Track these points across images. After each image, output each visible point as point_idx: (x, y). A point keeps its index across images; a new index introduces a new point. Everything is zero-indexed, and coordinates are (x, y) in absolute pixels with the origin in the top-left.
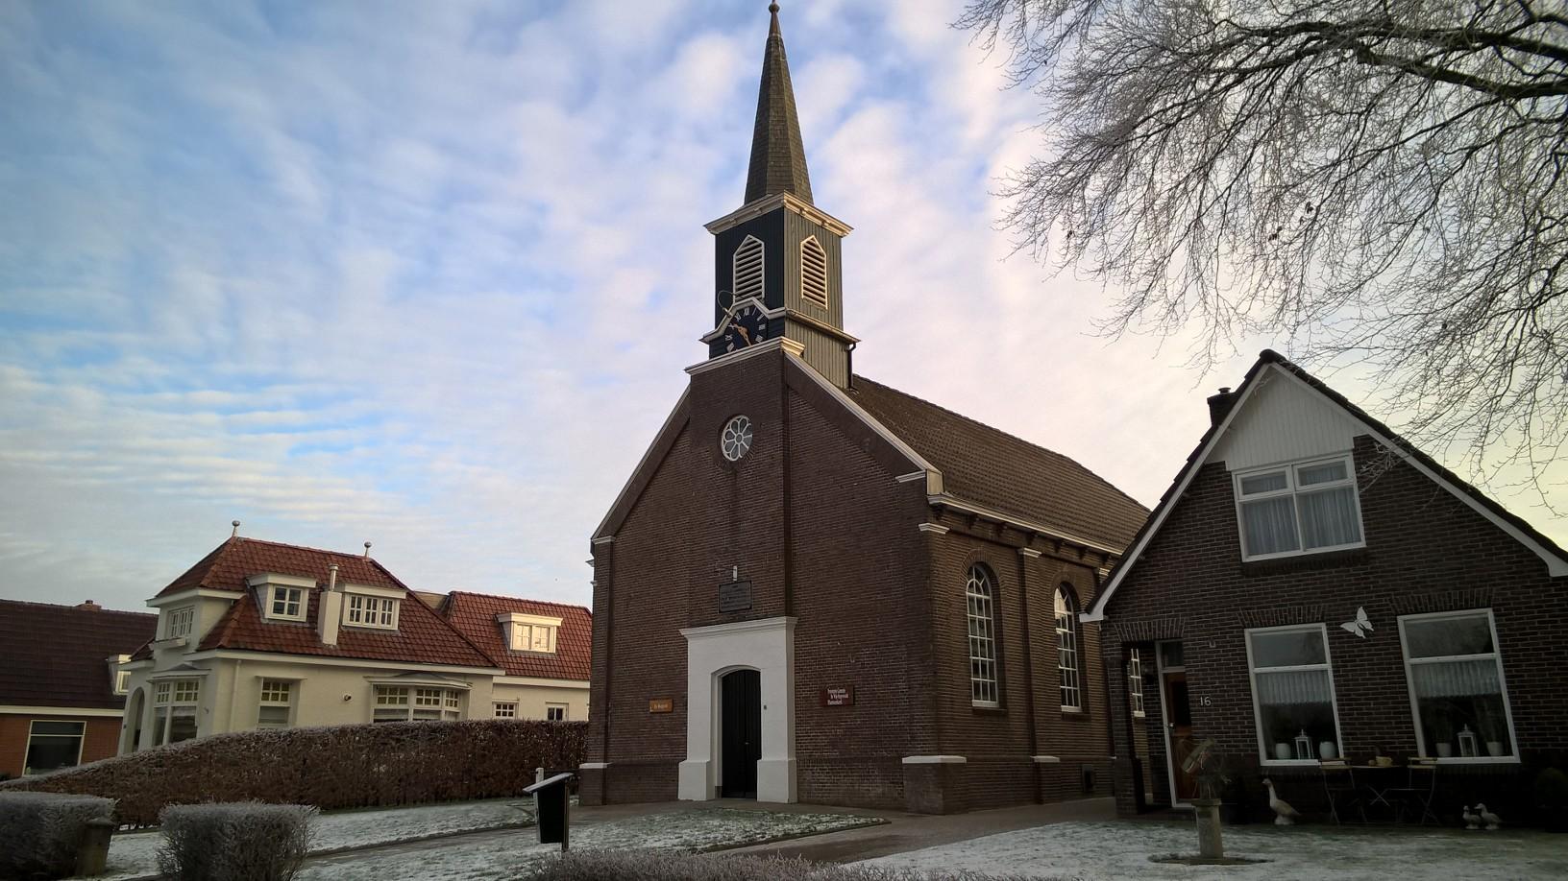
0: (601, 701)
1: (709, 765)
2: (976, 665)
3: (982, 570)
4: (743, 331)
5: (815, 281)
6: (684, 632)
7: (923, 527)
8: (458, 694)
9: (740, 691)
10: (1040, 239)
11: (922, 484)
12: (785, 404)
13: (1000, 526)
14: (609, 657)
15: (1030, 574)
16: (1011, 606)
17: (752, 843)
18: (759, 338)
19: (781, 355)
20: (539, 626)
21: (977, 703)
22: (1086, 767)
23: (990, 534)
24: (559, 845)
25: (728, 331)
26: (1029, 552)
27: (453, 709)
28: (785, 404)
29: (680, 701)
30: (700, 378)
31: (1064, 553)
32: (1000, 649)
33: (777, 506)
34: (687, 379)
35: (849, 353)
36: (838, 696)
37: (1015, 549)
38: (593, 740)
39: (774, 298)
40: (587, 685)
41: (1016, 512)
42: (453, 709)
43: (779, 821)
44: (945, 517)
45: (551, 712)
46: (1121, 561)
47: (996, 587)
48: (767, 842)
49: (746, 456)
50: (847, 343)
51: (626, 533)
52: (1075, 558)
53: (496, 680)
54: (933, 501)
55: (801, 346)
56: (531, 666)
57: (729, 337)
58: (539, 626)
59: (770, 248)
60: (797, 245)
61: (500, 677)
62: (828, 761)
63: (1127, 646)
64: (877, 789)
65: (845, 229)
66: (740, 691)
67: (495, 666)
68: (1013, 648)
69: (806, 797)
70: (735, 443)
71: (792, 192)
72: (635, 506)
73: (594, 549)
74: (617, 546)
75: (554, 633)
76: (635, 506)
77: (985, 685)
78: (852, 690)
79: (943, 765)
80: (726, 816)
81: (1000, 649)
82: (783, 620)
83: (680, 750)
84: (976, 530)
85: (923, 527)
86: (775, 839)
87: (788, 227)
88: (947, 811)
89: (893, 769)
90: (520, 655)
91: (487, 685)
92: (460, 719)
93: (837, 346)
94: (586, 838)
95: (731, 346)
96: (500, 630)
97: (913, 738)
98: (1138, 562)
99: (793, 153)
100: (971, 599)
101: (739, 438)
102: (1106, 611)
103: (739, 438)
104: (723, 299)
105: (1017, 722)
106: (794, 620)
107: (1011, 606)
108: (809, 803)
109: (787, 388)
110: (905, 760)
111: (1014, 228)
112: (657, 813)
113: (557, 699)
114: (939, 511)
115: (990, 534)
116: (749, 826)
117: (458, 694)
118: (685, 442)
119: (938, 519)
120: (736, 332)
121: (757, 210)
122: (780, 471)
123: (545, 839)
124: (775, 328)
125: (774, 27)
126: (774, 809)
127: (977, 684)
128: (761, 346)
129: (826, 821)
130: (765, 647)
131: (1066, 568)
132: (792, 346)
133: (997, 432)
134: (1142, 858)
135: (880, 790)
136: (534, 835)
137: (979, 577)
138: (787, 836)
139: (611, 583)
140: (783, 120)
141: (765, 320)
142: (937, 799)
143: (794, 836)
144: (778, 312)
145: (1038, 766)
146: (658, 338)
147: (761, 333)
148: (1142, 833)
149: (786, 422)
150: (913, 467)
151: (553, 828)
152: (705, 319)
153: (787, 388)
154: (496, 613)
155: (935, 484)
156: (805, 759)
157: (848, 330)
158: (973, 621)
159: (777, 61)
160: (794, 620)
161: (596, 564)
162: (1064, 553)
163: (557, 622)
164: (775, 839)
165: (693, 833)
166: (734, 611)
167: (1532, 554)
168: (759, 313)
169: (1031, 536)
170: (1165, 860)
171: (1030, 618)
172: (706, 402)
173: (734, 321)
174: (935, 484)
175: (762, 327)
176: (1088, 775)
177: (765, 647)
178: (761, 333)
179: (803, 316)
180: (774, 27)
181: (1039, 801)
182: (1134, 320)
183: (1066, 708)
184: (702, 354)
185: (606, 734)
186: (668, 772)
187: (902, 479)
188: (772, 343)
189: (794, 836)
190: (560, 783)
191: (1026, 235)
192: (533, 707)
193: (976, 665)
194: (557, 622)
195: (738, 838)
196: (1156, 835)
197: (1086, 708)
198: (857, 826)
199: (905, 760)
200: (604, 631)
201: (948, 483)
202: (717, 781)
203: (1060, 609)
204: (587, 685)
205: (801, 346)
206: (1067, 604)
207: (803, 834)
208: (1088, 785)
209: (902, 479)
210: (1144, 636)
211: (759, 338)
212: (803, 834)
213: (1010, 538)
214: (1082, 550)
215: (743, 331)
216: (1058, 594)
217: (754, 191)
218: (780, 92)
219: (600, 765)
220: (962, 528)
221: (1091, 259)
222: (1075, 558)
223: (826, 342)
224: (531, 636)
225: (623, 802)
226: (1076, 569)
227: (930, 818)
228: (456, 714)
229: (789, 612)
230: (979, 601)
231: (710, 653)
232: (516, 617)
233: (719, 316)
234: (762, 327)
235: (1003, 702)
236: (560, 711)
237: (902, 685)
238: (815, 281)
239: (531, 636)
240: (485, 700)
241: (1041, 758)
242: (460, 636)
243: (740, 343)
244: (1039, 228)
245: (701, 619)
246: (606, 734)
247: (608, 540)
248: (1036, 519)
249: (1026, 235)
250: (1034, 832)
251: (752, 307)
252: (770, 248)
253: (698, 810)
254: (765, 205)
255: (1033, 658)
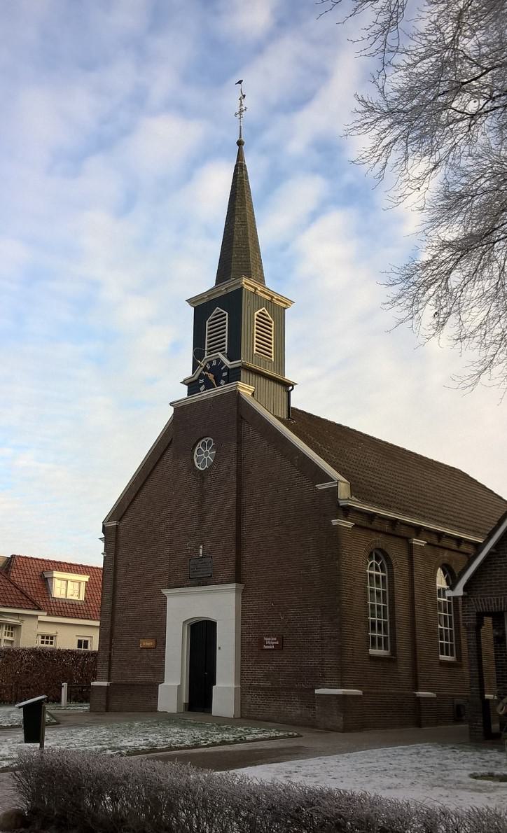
0: (108, 636)
1: (179, 687)
2: (373, 624)
3: (380, 554)
4: (211, 376)
5: (264, 338)
6: (164, 592)
7: (335, 522)
8: (13, 628)
9: (202, 633)
10: (416, 316)
11: (335, 491)
12: (239, 430)
13: (394, 522)
14: (113, 607)
15: (417, 558)
16: (401, 582)
17: (197, 746)
18: (222, 382)
19: (237, 395)
20: (72, 581)
21: (373, 651)
22: (458, 701)
23: (387, 528)
24: (38, 745)
25: (201, 376)
26: (418, 542)
27: (10, 638)
28: (239, 430)
29: (160, 640)
30: (180, 410)
31: (444, 542)
32: (392, 612)
33: (231, 503)
34: (171, 410)
35: (289, 393)
36: (271, 642)
37: (407, 539)
38: (102, 666)
39: (234, 354)
40: (98, 623)
41: (407, 512)
42: (10, 638)
43: (222, 731)
44: (351, 515)
45: (80, 642)
46: (478, 547)
47: (391, 567)
48: (208, 746)
49: (210, 467)
50: (287, 386)
51: (126, 520)
52: (454, 546)
53: (40, 618)
54: (342, 503)
55: (252, 388)
56: (67, 609)
57: (202, 381)
58: (72, 581)
59: (233, 317)
60: (253, 316)
61: (43, 616)
62: (262, 689)
63: (480, 616)
64: (296, 711)
65: (288, 303)
66: (202, 633)
67: (39, 609)
68: (402, 610)
69: (247, 715)
70: (204, 457)
71: (249, 276)
72: (133, 500)
73: (105, 530)
74: (113, 533)
75: (83, 585)
76: (133, 500)
77: (380, 639)
78: (281, 639)
79: (344, 696)
80: (184, 726)
81: (392, 612)
82: (233, 586)
83: (159, 675)
84: (376, 525)
85: (335, 522)
86: (214, 744)
87: (246, 302)
88: (346, 729)
89: (308, 697)
90: (58, 601)
91: (34, 623)
92: (14, 646)
93: (279, 388)
94: (54, 740)
95: (203, 388)
96: (45, 583)
97: (323, 676)
98: (490, 554)
99: (251, 248)
100: (371, 575)
101: (206, 454)
102: (465, 589)
103: (206, 454)
104: (198, 354)
105: (403, 667)
106: (242, 586)
107: (401, 582)
108: (248, 718)
109: (240, 419)
110: (317, 691)
111: (399, 308)
112: (136, 721)
113: (84, 634)
114: (347, 511)
115: (387, 528)
116: (197, 733)
117: (13, 628)
118: (169, 456)
119: (346, 517)
120: (206, 377)
121: (223, 290)
122: (234, 478)
123: (28, 739)
124: (234, 375)
125: (240, 157)
126: (222, 722)
127: (373, 638)
128: (224, 388)
129: (255, 733)
130: (220, 605)
131: (446, 554)
132: (245, 389)
133: (403, 450)
134: (464, 775)
135: (299, 712)
136: (20, 735)
137: (378, 559)
138: (223, 743)
139: (116, 554)
140: (244, 224)
141: (227, 369)
142: (339, 721)
143: (228, 743)
144: (236, 364)
145: (419, 699)
146: (157, 374)
147: (224, 378)
148: (478, 754)
149: (239, 443)
150: (326, 478)
151: (33, 729)
152: (186, 369)
153: (240, 419)
154: (42, 571)
155: (344, 491)
156: (247, 687)
157: (289, 376)
158: (372, 591)
159: (242, 182)
160: (242, 586)
161: (106, 540)
162: (444, 542)
163: (86, 578)
164: (214, 744)
165: (157, 737)
166: (199, 578)
167: (32, 698)
168: (223, 364)
169: (418, 530)
170: (483, 777)
171: (417, 590)
172: (184, 426)
173: (205, 369)
174: (344, 491)
175: (225, 374)
176: (459, 707)
177: (220, 605)
178: (224, 378)
179: (254, 366)
180: (240, 157)
181: (419, 725)
182: (484, 377)
183: (443, 657)
184: (182, 393)
185: (110, 662)
186: (150, 691)
187: (321, 487)
188: (231, 386)
189: (228, 743)
190: (42, 699)
191: (406, 313)
192: (66, 639)
193: (373, 624)
194: (86, 578)
195: (187, 743)
196: (487, 757)
197: (459, 658)
198: (276, 738)
199: (317, 691)
200: (110, 589)
201: (355, 490)
202: (185, 699)
203: (441, 582)
204: (98, 623)
205: (252, 388)
206: (447, 580)
207: (235, 742)
208: (458, 715)
209: (321, 487)
210: (493, 608)
211: (222, 382)
212: (235, 742)
213: (403, 531)
214: (459, 541)
215: (211, 376)
216: (440, 571)
217: (224, 271)
218: (243, 203)
219: (105, 684)
220: (365, 524)
221: (451, 329)
222: (454, 546)
223: (272, 385)
224: (67, 588)
225: (120, 710)
226: (454, 554)
227: (333, 734)
228: (12, 642)
229: (238, 580)
230: (377, 577)
231: (182, 607)
232: (56, 574)
233: (195, 366)
234: (225, 374)
235: (394, 651)
236: (86, 642)
237: (317, 637)
238: (264, 338)
239: (67, 588)
240: (33, 633)
241: (421, 694)
242: (16, 587)
243: (209, 385)
244: (415, 308)
245: (176, 583)
246: (110, 662)
247: (114, 523)
248: (424, 518)
249: (406, 313)
250: (398, 749)
251: (218, 360)
252: (233, 317)
253: (169, 719)
254: (229, 286)
255: (418, 619)
